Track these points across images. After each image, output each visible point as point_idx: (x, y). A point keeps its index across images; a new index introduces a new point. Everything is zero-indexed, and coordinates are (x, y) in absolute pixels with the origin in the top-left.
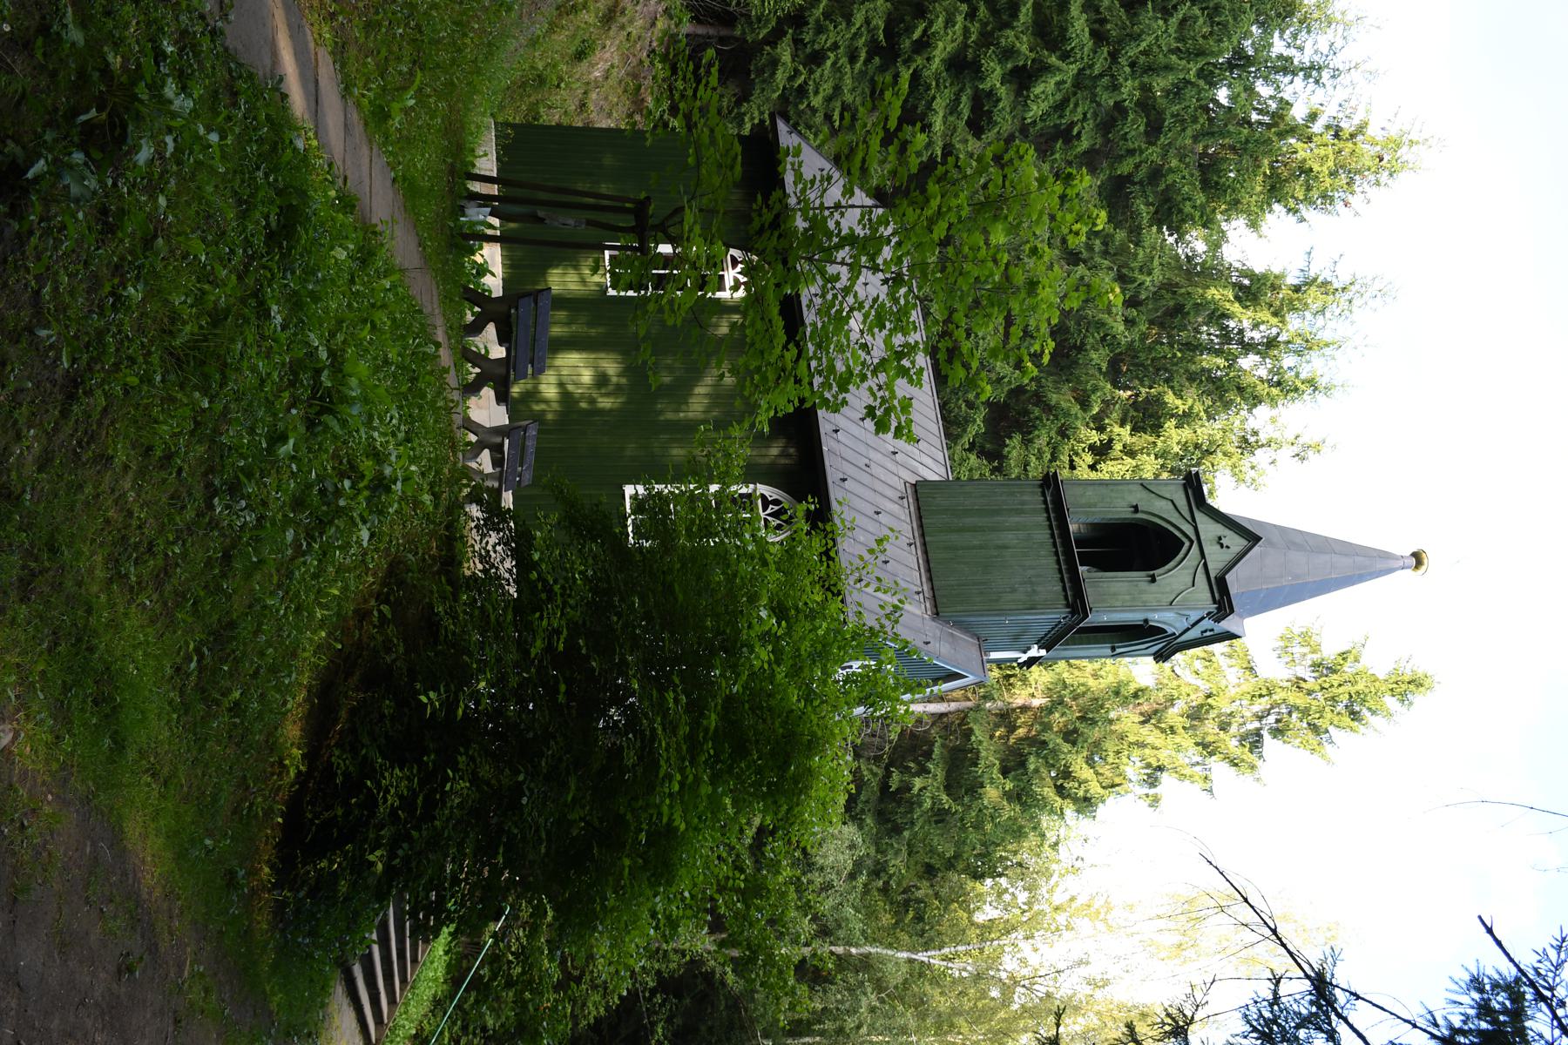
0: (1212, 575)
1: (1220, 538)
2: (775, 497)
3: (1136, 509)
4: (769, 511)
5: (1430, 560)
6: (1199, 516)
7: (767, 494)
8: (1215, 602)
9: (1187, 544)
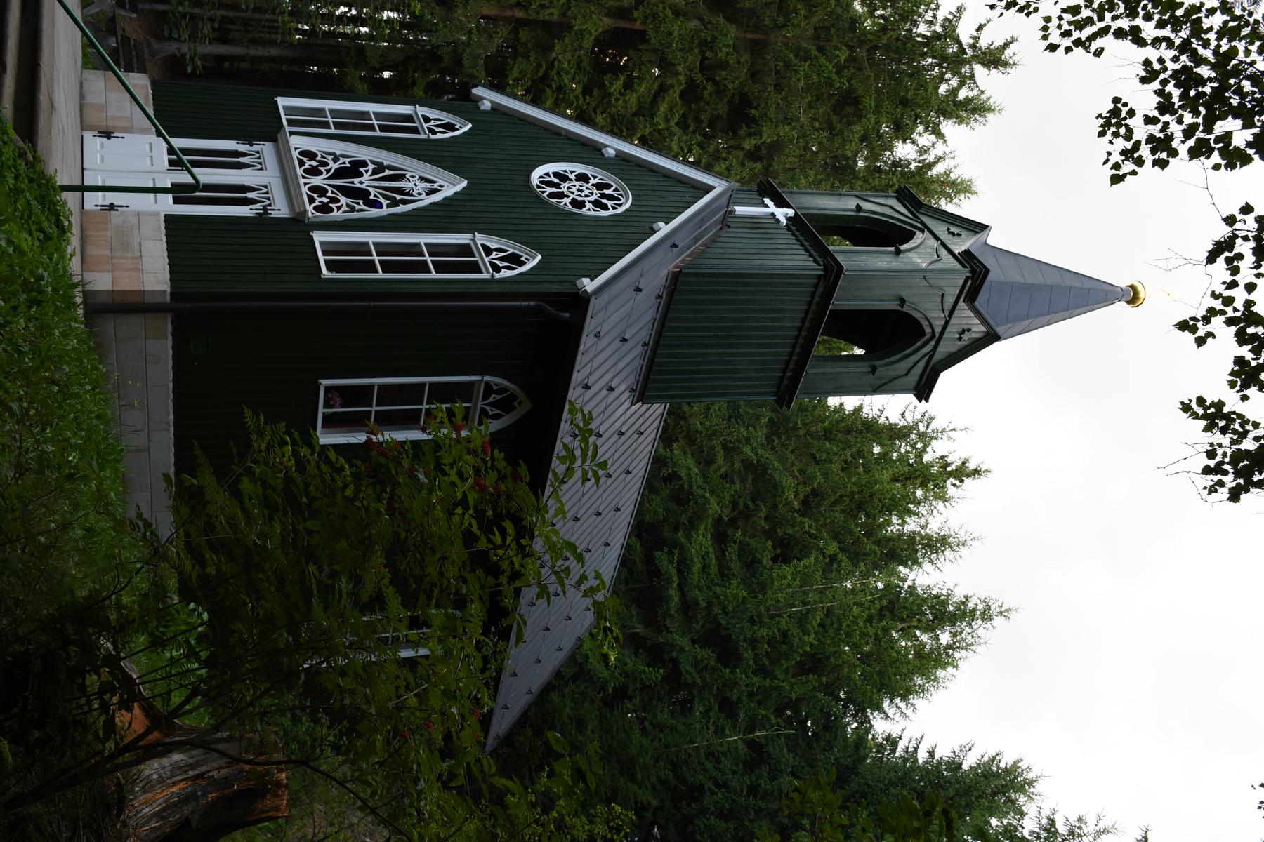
3: (902, 301)
9: (928, 336)
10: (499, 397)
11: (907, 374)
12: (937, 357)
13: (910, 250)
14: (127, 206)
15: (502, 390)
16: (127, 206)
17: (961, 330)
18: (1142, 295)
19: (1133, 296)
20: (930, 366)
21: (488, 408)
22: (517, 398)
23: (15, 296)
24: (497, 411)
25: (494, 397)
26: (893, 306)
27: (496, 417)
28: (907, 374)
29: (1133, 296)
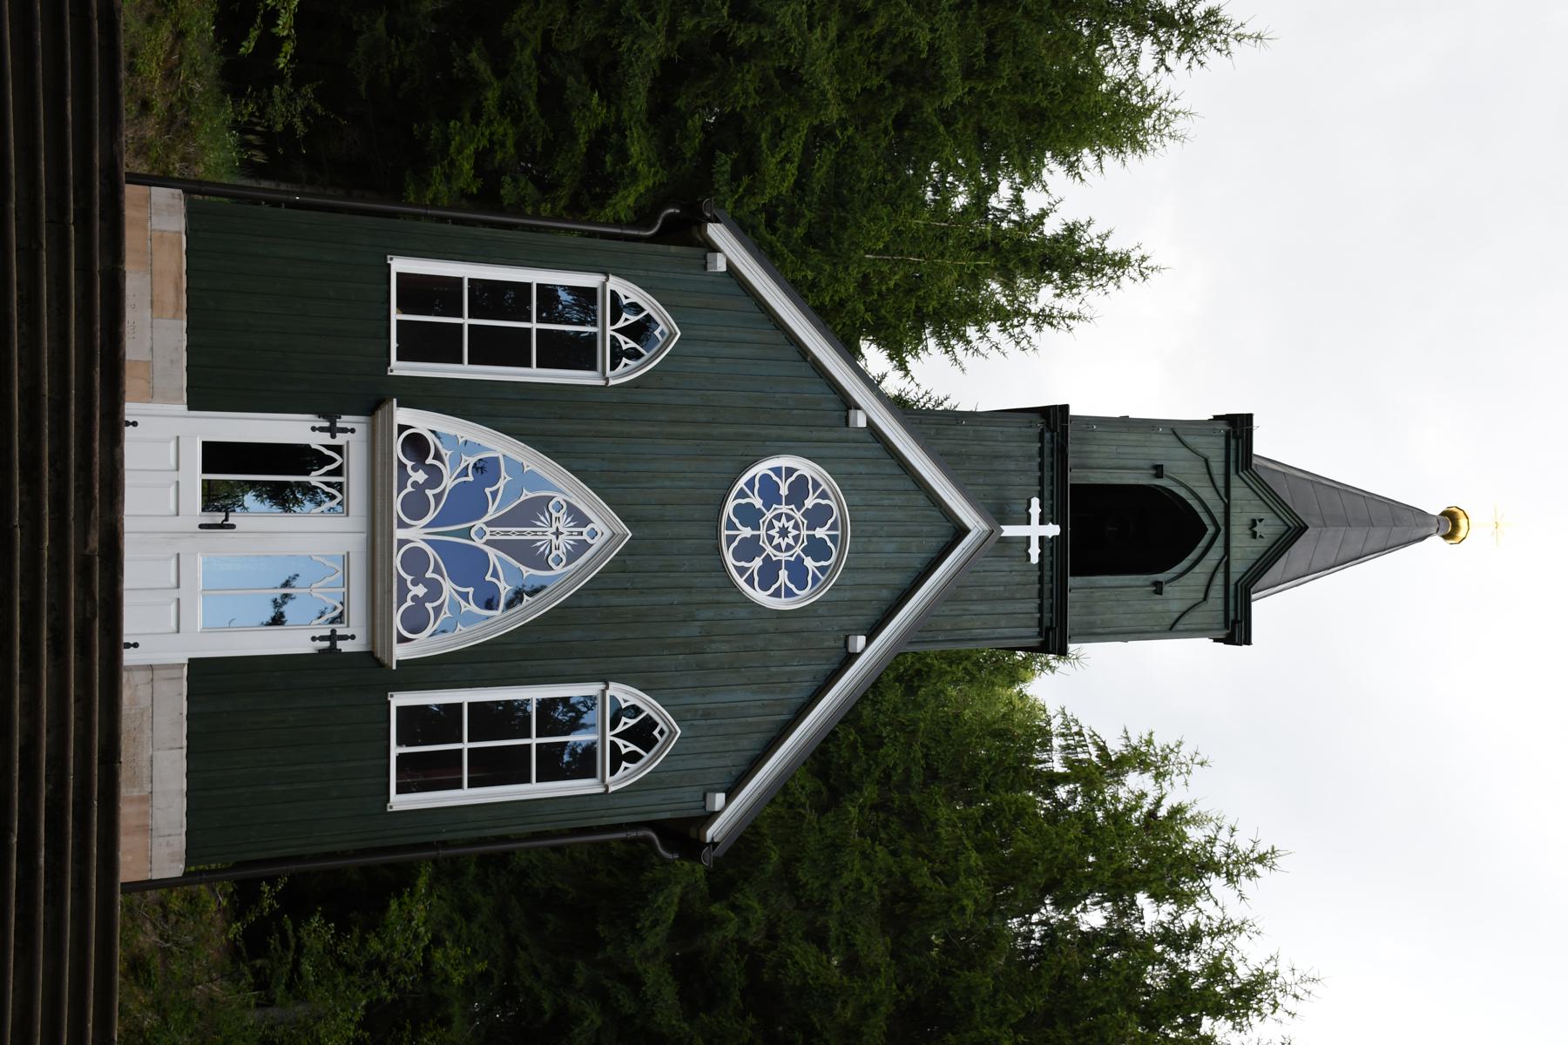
0: (1234, 577)
1: (1254, 523)
2: (632, 701)
3: (1159, 471)
4: (620, 324)
5: (1474, 529)
6: (1239, 490)
7: (620, 697)
8: (1226, 627)
9: (1211, 530)
10: (632, 722)
11: (1205, 599)
12: (1238, 568)
13: (890, 568)
14: (313, 429)
15: (636, 710)
16: (313, 429)
17: (1250, 523)
18: (1461, 534)
19: (1449, 525)
20: (1232, 588)
21: (620, 742)
22: (656, 724)
23: (1088, 120)
24: (633, 747)
25: (627, 722)
26: (1145, 479)
27: (633, 757)
28: (1205, 599)
29: (1449, 525)
